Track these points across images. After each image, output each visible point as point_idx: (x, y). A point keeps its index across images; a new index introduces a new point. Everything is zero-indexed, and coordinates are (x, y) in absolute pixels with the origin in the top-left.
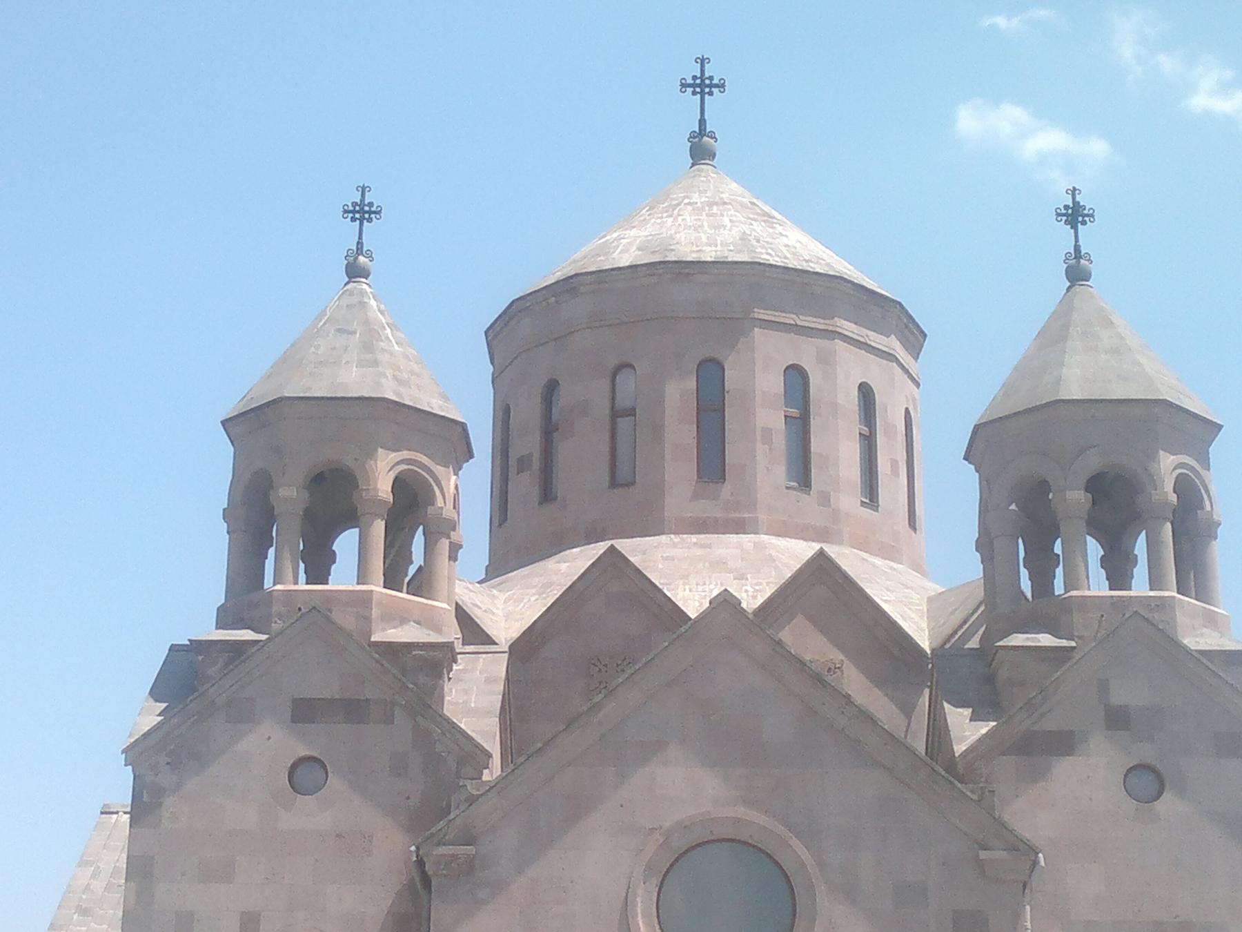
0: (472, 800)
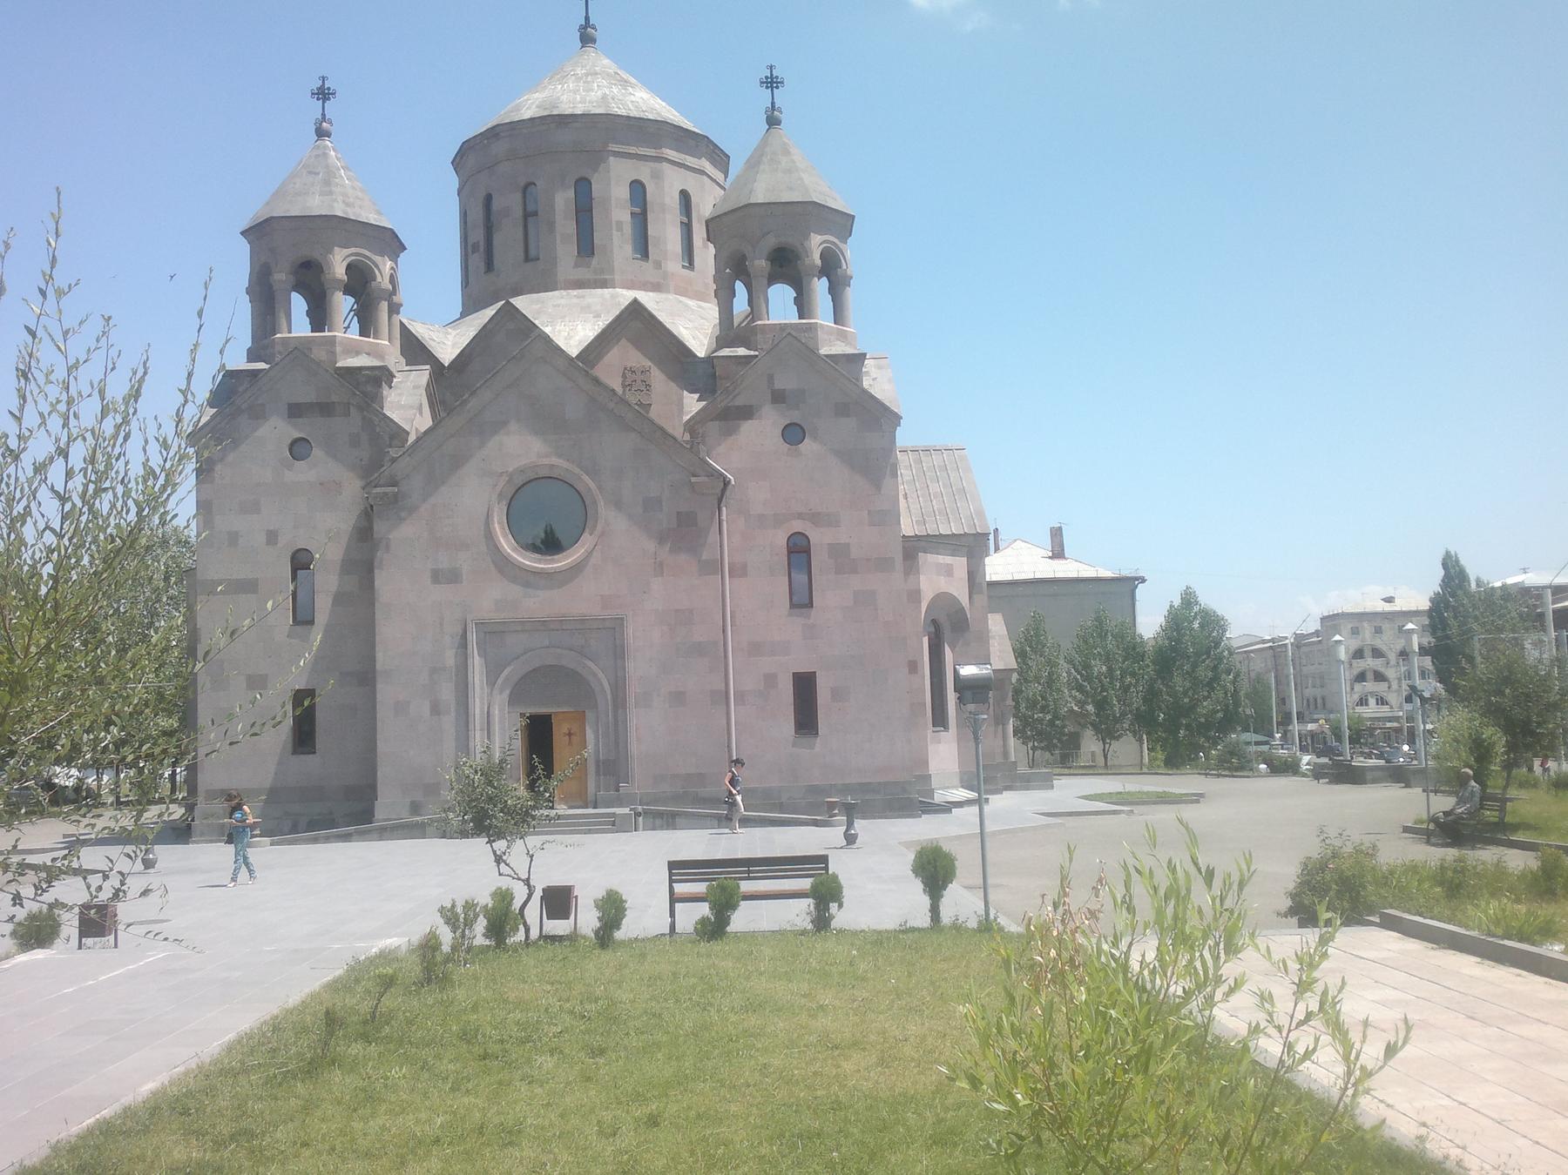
0: (394, 460)
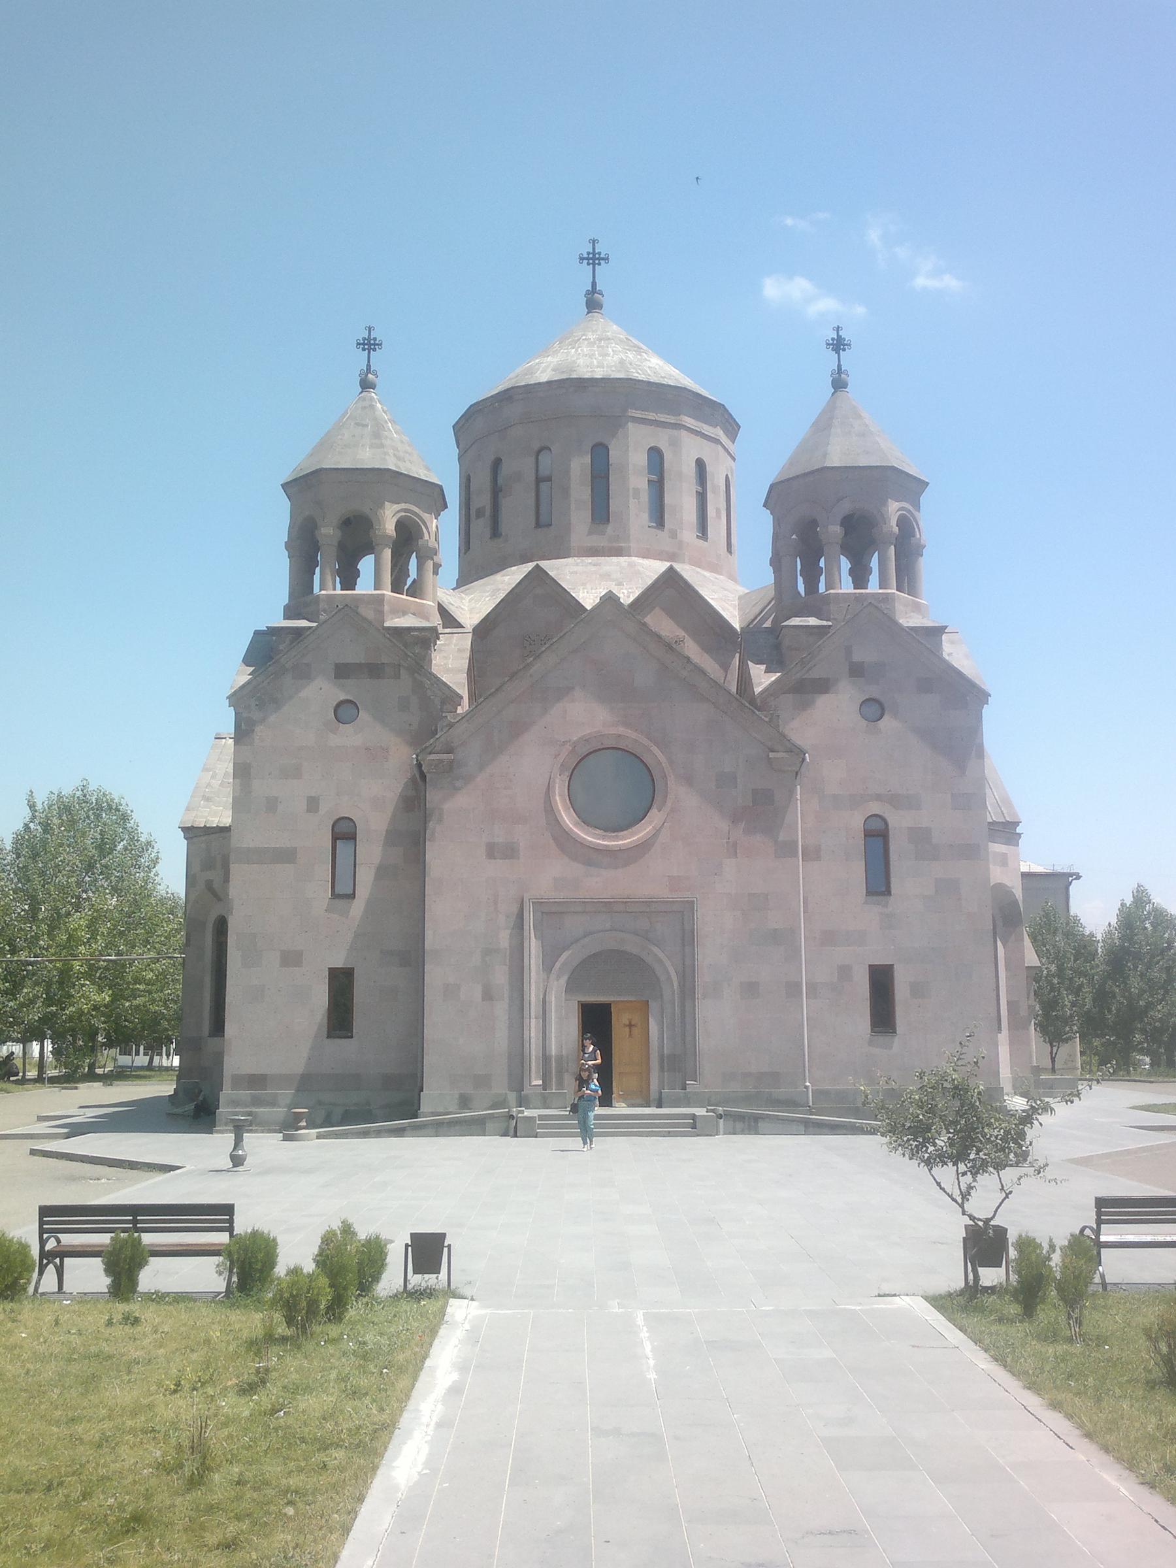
0: (451, 725)
